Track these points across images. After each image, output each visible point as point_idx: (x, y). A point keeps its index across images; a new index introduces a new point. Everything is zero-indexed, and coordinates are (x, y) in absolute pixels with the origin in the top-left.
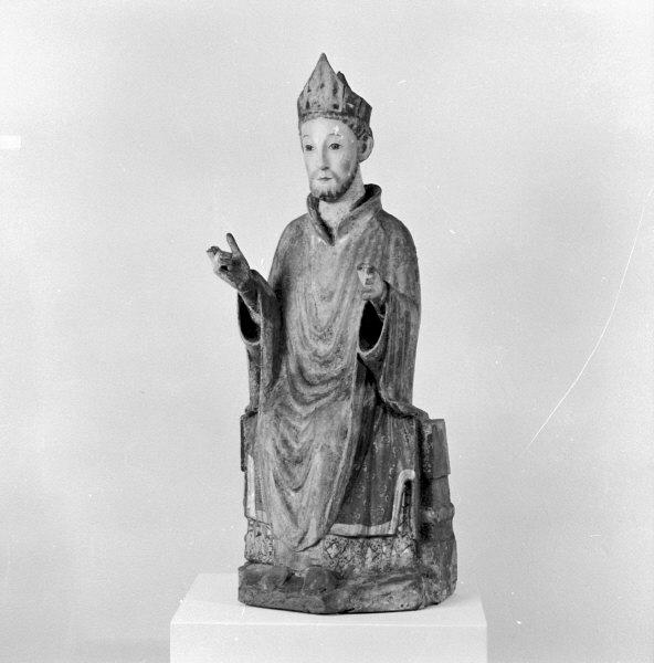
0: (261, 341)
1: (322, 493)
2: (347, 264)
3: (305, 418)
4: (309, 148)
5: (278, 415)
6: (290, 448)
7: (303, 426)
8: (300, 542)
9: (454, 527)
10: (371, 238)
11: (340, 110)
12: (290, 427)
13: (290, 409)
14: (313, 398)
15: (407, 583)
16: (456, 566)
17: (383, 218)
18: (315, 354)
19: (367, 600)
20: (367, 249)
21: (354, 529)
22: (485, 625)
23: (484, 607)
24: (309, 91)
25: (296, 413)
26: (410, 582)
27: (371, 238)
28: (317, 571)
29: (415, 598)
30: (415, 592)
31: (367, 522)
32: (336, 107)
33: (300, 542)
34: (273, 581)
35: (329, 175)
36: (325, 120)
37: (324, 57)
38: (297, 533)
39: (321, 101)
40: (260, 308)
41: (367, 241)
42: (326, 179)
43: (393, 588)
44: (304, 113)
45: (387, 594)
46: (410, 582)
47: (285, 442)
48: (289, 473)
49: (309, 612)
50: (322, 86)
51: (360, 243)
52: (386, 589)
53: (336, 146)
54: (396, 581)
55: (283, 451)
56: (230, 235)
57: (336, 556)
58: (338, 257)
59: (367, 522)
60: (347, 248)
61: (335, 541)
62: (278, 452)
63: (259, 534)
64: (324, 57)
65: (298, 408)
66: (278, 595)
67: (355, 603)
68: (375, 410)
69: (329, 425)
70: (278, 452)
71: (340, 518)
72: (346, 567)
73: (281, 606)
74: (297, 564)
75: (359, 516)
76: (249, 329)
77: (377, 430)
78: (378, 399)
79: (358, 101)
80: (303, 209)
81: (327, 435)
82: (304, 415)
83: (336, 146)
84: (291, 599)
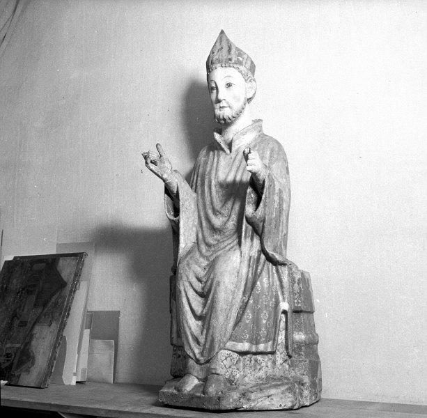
1: (311, 397)
9: (319, 350)
15: (283, 388)
16: (321, 380)
19: (254, 401)
21: (245, 346)
26: (286, 387)
29: (291, 399)
30: (290, 395)
37: (222, 32)
40: (286, 295)
43: (273, 391)
45: (269, 397)
46: (286, 387)
52: (266, 393)
54: (276, 386)
57: (230, 367)
61: (229, 356)
63: (179, 356)
64: (222, 32)
68: (259, 258)
72: (238, 376)
77: (262, 270)
78: (263, 251)
79: (245, 56)
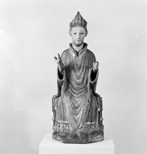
0: (64, 79)
2: (83, 61)
3: (78, 98)
4: (75, 34)
5: (71, 97)
6: (75, 105)
7: (77, 100)
8: (78, 127)
10: (87, 55)
11: (83, 25)
12: (74, 100)
13: (73, 95)
14: (78, 93)
17: (88, 51)
18: (76, 82)
20: (87, 58)
21: (89, 123)
22: (114, 147)
23: (113, 141)
24: (75, 20)
25: (75, 97)
26: (101, 134)
27: (87, 55)
28: (82, 133)
31: (91, 122)
32: (82, 24)
33: (78, 127)
34: (72, 136)
35: (80, 40)
36: (80, 27)
37: (78, 12)
38: (77, 125)
39: (78, 22)
41: (87, 56)
42: (79, 41)
44: (72, 26)
46: (101, 134)
47: (73, 104)
48: (75, 111)
49: (82, 143)
50: (79, 19)
51: (85, 56)
53: (82, 33)
55: (73, 106)
56: (59, 54)
58: (80, 60)
59: (91, 122)
60: (82, 57)
62: (72, 106)
64: (78, 12)
65: (75, 95)
66: (74, 140)
67: (92, 141)
69: (86, 99)
70: (72, 106)
71: (87, 121)
73: (75, 143)
74: (76, 132)
75: (90, 120)
76: (60, 76)
80: (68, 47)
81: (85, 101)
82: (77, 97)
83: (82, 33)
84: (78, 141)
